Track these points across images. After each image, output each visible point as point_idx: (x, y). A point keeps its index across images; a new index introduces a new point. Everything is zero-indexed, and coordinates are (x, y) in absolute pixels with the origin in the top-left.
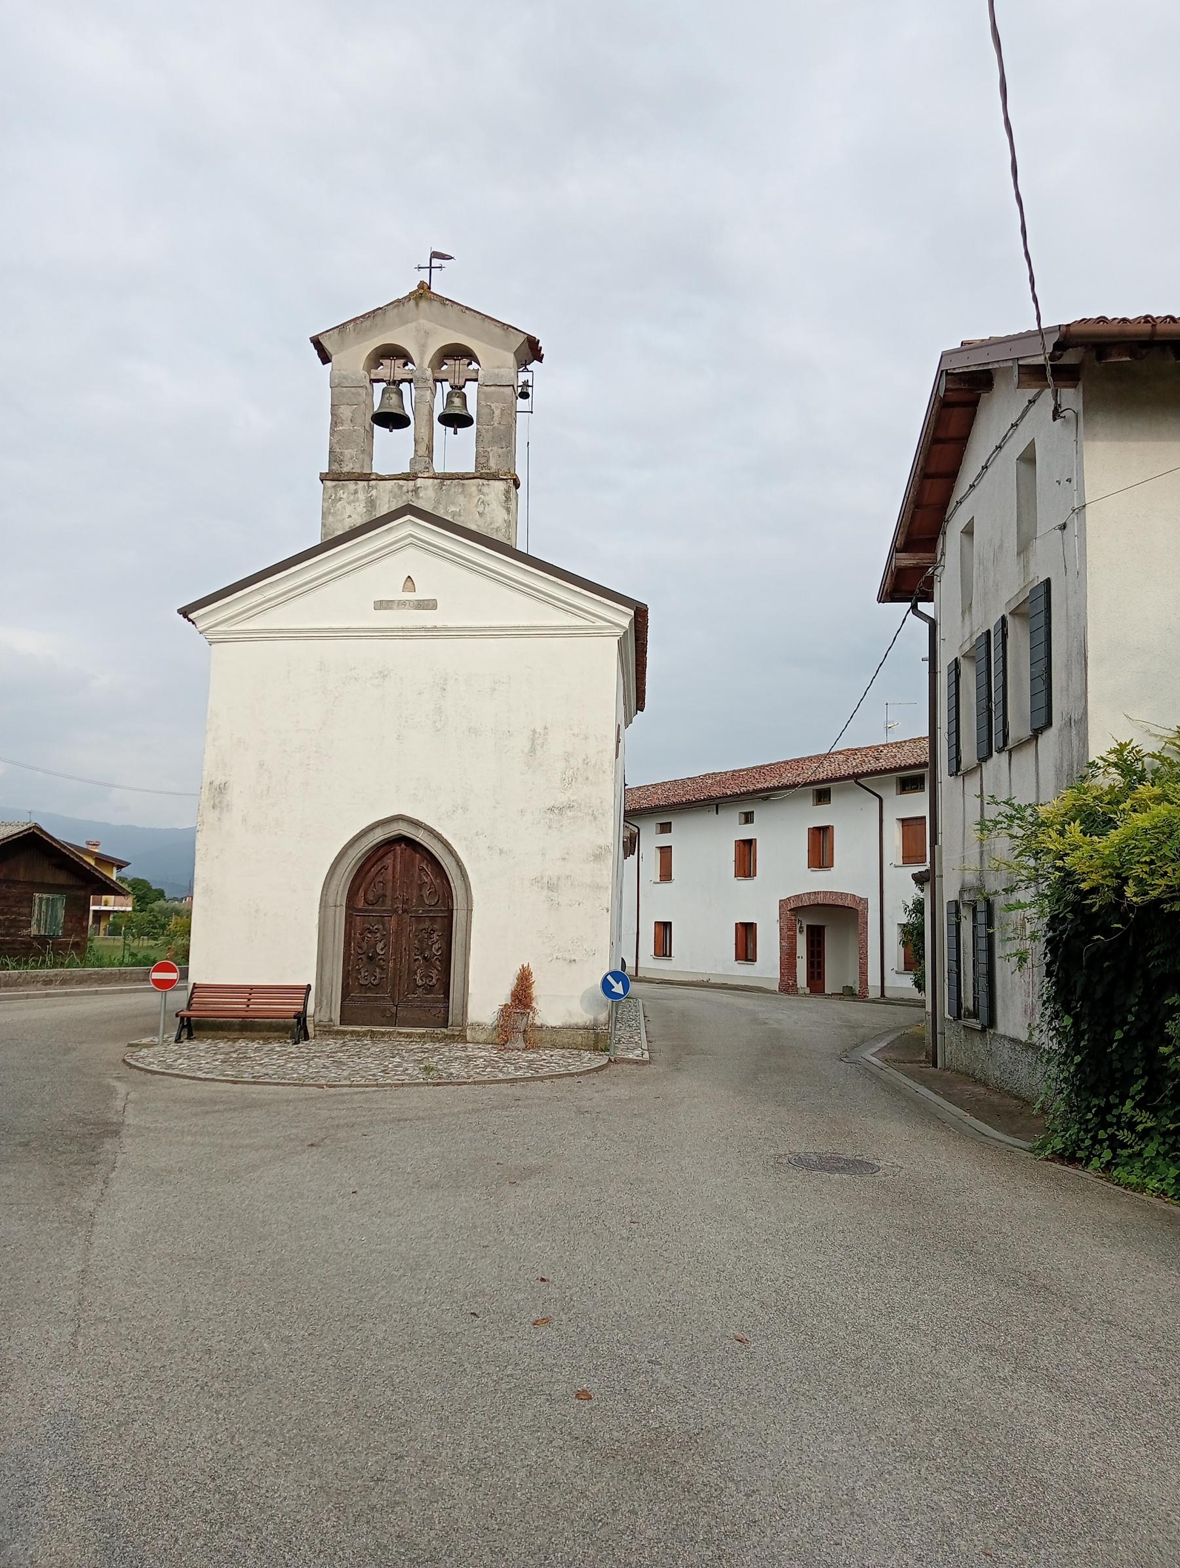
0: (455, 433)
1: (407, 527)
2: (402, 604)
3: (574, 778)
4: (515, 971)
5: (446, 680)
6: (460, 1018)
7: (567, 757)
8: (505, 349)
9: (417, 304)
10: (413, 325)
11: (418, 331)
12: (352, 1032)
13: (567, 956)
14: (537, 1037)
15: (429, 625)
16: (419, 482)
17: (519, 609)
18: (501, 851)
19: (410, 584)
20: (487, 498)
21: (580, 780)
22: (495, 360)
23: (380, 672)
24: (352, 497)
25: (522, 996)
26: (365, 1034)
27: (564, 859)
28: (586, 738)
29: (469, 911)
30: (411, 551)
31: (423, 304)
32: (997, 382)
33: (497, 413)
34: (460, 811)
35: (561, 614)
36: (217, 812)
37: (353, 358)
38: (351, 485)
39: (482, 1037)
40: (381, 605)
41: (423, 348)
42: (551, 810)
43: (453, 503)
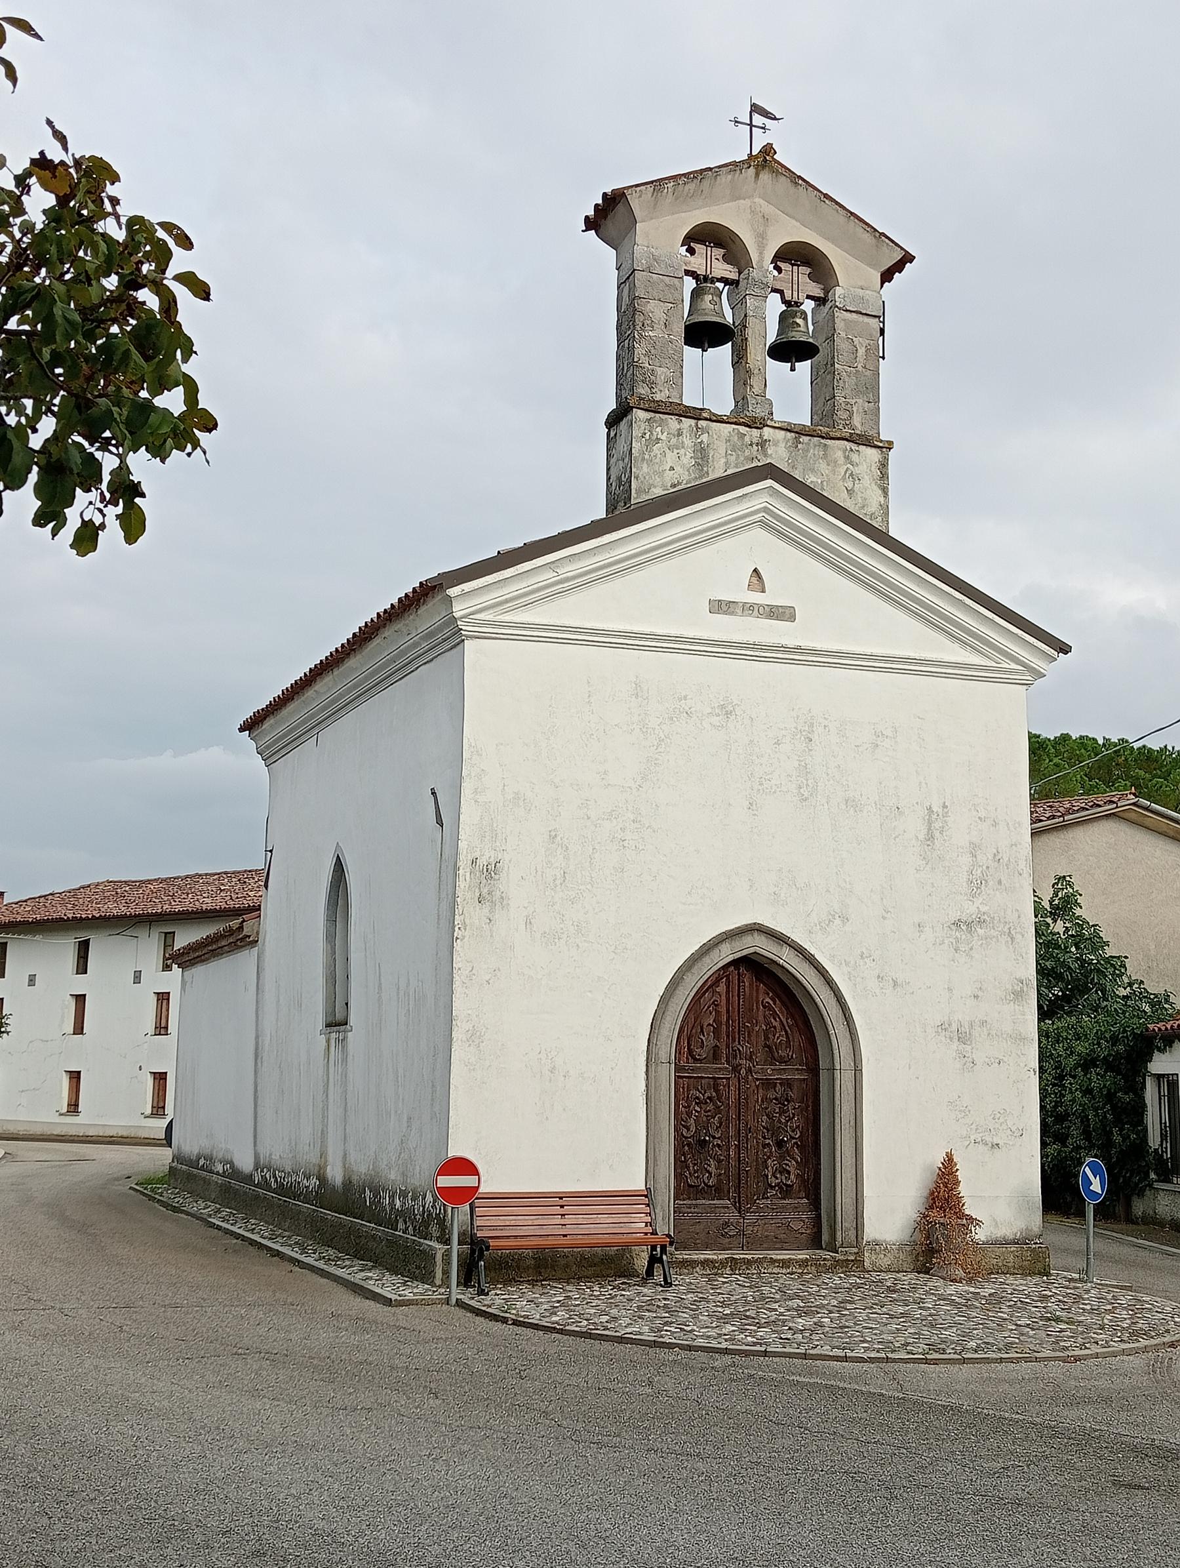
0: (793, 369)
2: (749, 609)
4: (939, 1159)
5: (812, 725)
6: (852, 1233)
7: (974, 849)
8: (869, 265)
9: (757, 175)
10: (748, 202)
12: (705, 1263)
13: (988, 1139)
14: (982, 1265)
15: (791, 643)
16: (767, 432)
17: (910, 637)
18: (895, 983)
19: (755, 580)
20: (856, 470)
21: (991, 883)
22: (852, 276)
23: (722, 707)
24: (674, 441)
25: (943, 1195)
26: (723, 1264)
27: (976, 997)
28: (995, 824)
29: (858, 1071)
30: (759, 533)
31: (765, 176)
33: (861, 351)
34: (838, 921)
36: (486, 910)
37: (660, 234)
38: (673, 422)
39: (885, 1262)
40: (720, 607)
41: (761, 238)
42: (957, 924)
43: (812, 470)
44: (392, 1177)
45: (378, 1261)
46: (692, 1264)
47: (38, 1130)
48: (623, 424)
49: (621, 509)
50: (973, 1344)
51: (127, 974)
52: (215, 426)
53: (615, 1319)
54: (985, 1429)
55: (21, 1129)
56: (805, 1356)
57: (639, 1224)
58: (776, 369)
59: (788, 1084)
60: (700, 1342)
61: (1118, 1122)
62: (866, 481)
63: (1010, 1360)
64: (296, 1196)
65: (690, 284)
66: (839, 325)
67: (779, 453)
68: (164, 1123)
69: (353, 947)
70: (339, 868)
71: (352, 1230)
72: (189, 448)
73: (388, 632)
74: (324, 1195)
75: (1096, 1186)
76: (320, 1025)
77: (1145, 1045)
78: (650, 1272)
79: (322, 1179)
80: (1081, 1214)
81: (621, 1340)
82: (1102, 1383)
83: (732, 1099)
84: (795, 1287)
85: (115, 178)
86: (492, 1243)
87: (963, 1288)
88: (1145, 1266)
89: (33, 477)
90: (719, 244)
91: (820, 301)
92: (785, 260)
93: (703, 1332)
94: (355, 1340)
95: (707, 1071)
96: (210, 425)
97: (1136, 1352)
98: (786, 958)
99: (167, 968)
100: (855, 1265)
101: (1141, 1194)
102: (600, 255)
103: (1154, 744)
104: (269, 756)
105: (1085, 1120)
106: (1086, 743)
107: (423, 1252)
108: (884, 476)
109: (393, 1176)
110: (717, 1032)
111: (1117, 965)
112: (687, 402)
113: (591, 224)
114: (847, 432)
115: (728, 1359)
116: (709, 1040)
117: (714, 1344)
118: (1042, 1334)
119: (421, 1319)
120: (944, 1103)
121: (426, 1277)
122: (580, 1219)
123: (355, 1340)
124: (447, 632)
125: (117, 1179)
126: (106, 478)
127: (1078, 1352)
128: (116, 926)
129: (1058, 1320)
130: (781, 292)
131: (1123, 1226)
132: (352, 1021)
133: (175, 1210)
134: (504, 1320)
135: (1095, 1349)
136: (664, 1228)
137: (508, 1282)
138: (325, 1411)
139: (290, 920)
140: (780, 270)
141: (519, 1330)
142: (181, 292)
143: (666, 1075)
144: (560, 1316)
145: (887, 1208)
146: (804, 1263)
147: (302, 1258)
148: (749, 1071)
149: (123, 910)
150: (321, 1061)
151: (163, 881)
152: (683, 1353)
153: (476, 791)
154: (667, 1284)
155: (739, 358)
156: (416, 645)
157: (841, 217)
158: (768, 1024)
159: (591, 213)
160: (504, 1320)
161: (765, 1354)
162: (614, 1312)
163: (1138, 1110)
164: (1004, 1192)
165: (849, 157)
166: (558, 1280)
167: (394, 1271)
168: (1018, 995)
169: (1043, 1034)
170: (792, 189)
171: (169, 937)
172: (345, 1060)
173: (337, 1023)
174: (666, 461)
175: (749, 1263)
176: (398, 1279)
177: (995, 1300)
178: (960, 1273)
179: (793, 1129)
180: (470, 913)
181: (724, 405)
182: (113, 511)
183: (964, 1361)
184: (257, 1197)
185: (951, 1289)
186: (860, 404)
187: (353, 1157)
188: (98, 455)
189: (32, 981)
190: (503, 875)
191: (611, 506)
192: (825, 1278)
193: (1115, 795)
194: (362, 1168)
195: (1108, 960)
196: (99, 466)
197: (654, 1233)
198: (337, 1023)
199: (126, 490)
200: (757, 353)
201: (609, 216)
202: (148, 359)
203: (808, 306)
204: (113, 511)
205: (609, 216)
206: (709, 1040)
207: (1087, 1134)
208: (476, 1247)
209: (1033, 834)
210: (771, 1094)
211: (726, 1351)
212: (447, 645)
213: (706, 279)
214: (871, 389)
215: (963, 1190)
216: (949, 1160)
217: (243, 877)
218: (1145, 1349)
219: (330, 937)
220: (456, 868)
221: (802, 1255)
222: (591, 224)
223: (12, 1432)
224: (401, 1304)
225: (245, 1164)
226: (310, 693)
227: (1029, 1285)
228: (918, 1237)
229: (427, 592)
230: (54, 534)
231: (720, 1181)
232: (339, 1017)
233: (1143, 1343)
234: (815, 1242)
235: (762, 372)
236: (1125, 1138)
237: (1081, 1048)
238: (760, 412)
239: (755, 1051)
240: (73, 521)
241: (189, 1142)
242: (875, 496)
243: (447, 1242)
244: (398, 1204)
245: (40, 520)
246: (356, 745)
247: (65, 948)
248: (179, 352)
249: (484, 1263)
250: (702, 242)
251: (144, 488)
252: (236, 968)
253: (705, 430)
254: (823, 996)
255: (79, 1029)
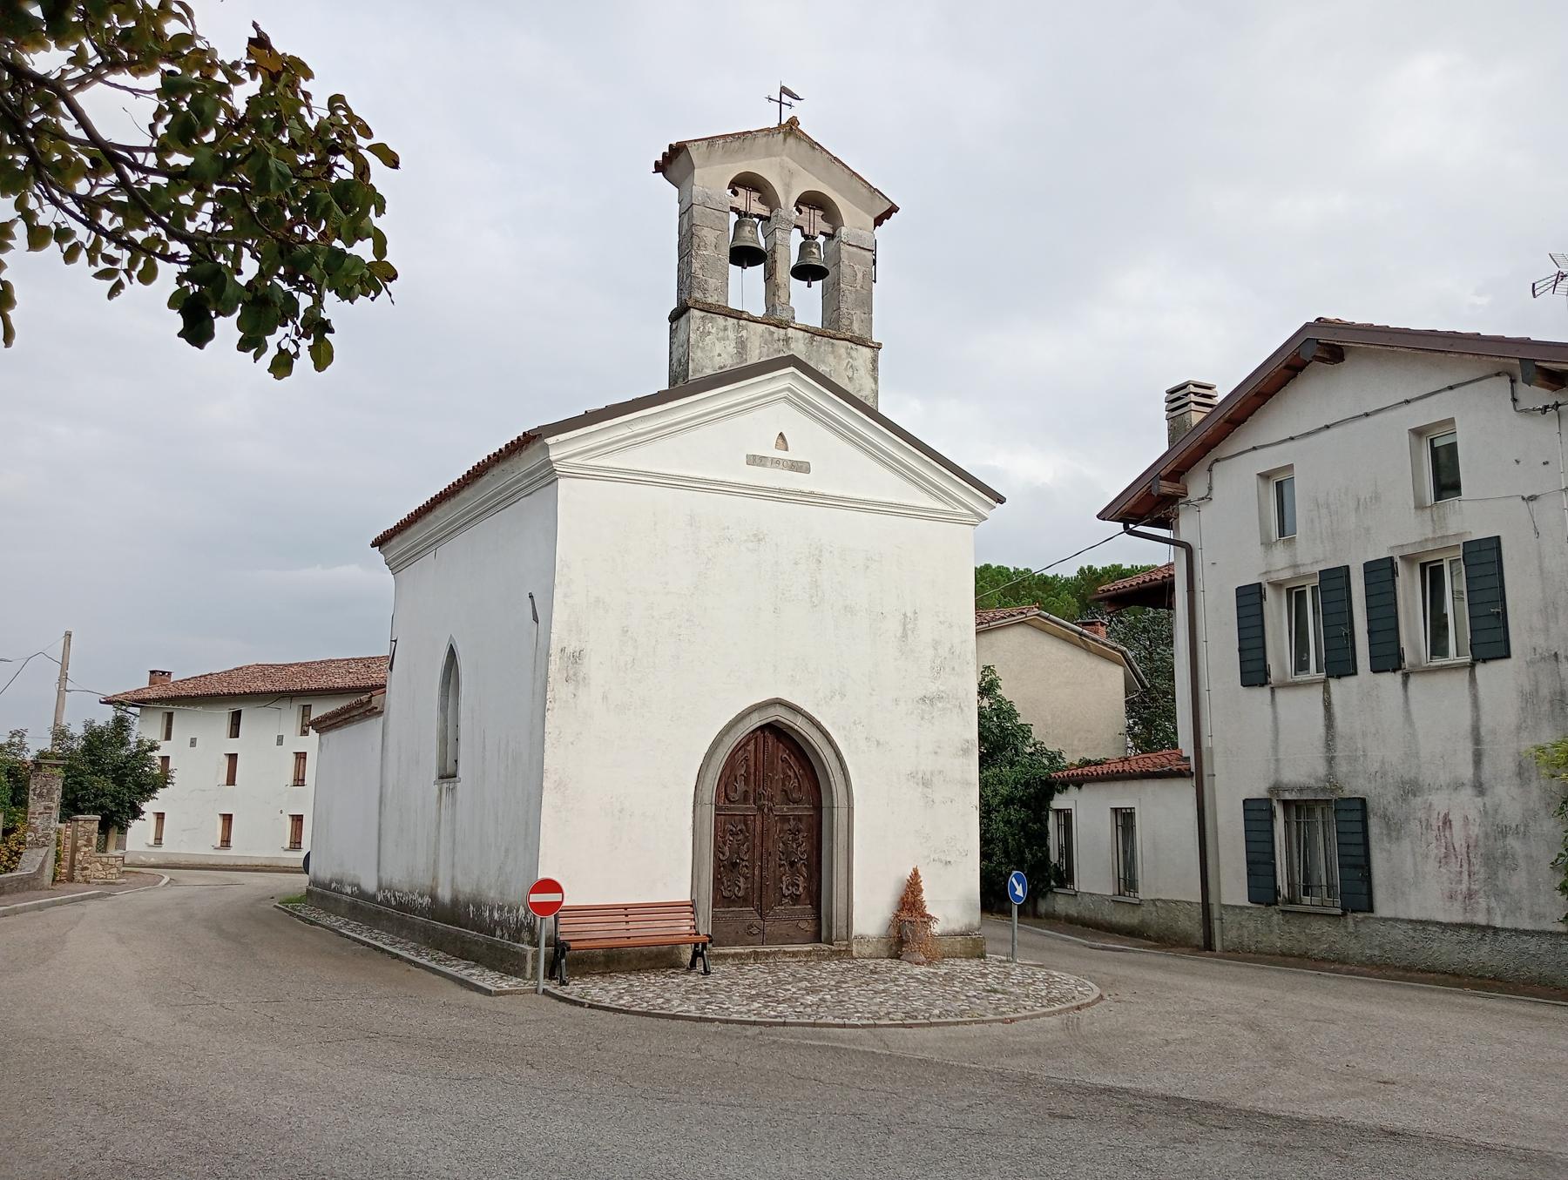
1: (785, 379)
3: (942, 668)
4: (909, 872)
7: (936, 644)
11: (782, 167)
12: (734, 956)
15: (807, 490)
17: (891, 488)
20: (855, 363)
22: (854, 220)
25: (910, 900)
26: (748, 956)
28: (951, 626)
29: (850, 809)
30: (783, 406)
31: (791, 141)
32: (1348, 359)
33: (860, 275)
35: (925, 495)
36: (572, 687)
37: (713, 179)
38: (720, 320)
39: (867, 951)
40: (754, 460)
41: (788, 187)
42: (923, 699)
44: (492, 894)
45: (478, 961)
46: (725, 956)
47: (197, 861)
48: (683, 320)
49: (680, 384)
50: (937, 1012)
51: (271, 740)
52: (396, 276)
53: (668, 1001)
54: (951, 1076)
55: (183, 861)
56: (814, 1025)
57: (685, 927)
58: (797, 285)
59: (798, 818)
60: (735, 1017)
61: (1029, 845)
62: (862, 371)
63: (965, 1023)
64: (412, 911)
65: (734, 217)
66: (844, 255)
67: (799, 348)
68: (302, 854)
69: (462, 715)
70: (452, 653)
71: (459, 938)
72: (372, 294)
73: (495, 471)
74: (437, 910)
75: (1019, 892)
76: (434, 777)
77: (1050, 788)
78: (693, 964)
79: (434, 897)
80: (1009, 913)
81: (674, 1017)
82: (1032, 1038)
83: (758, 829)
84: (803, 972)
85: (309, 75)
86: (572, 945)
87: (924, 969)
88: (1051, 950)
89: (238, 313)
90: (756, 190)
91: (830, 237)
92: (804, 204)
93: (737, 1010)
94: (465, 1024)
95: (739, 809)
96: (392, 275)
97: (1053, 1013)
98: (800, 724)
99: (305, 733)
100: (846, 954)
101: (1044, 896)
102: (666, 192)
103: (1049, 573)
104: (395, 567)
105: (1005, 841)
106: (1001, 571)
107: (517, 953)
108: (875, 369)
109: (492, 895)
110: (747, 782)
111: (1025, 731)
112: (732, 305)
113: (659, 167)
114: (848, 334)
115: (756, 1029)
116: (741, 786)
117: (745, 1018)
118: (985, 1002)
119: (516, 1004)
120: (910, 832)
121: (518, 972)
122: (641, 925)
123: (465, 1024)
124: (544, 472)
125: (263, 899)
126: (302, 314)
127: (1012, 1015)
128: (264, 700)
129: (995, 991)
130: (801, 228)
131: (1031, 920)
132: (461, 774)
133: (312, 923)
134: (582, 1005)
135: (1025, 1013)
136: (705, 929)
137: (584, 974)
138: (444, 1082)
139: (411, 698)
140: (800, 212)
141: (594, 1012)
142: (373, 161)
143: (709, 812)
144: (626, 1000)
145: (869, 911)
146: (808, 953)
147: (418, 959)
148: (770, 809)
149: (270, 687)
150: (434, 806)
151: (301, 665)
152: (723, 1026)
153: (565, 596)
154: (707, 972)
155: (769, 276)
156: (518, 481)
157: (846, 176)
158: (784, 773)
159: (660, 159)
160: (582, 1005)
161: (784, 1024)
162: (667, 995)
163: (1044, 834)
164: (953, 897)
165: (857, 129)
166: (623, 972)
167: (492, 968)
168: (966, 752)
169: (984, 784)
170: (810, 152)
171: (306, 710)
172: (454, 804)
173: (448, 776)
174: (715, 348)
175: (767, 955)
176: (496, 975)
177: (949, 978)
178: (922, 958)
179: (802, 851)
180: (558, 690)
181: (759, 310)
182: (305, 344)
183: (931, 1024)
184: (379, 912)
185: (917, 970)
186: (857, 315)
187: (460, 878)
188: (295, 294)
189: (193, 743)
190: (586, 661)
191: (673, 380)
192: (824, 964)
193: (1025, 608)
194: (467, 888)
195: (1019, 727)
196: (295, 304)
197: (697, 934)
198: (448, 776)
199: (317, 327)
200: (783, 273)
201: (673, 162)
202: (346, 212)
203: (821, 239)
204: (305, 344)
205: (673, 162)
206: (741, 786)
207: (1006, 853)
208: (559, 949)
209: (978, 633)
210: (786, 827)
211: (755, 1023)
212: (545, 482)
213: (746, 214)
214: (866, 303)
215: (925, 896)
216: (916, 873)
217: (367, 662)
218: (1060, 1012)
219: (443, 708)
220: (548, 655)
221: (808, 948)
222: (659, 167)
223: (183, 1107)
224: (498, 994)
225: (370, 885)
226: (430, 517)
227: (973, 965)
228: (894, 933)
229: (528, 440)
230: (256, 358)
231: (747, 893)
232: (449, 771)
233: (1058, 1007)
234: (817, 938)
235: (787, 286)
236: (1034, 856)
237: (1004, 790)
238: (785, 316)
239: (774, 792)
240: (272, 352)
241: (323, 869)
242: (868, 383)
243: (537, 945)
244: (496, 916)
245: (243, 346)
246: (466, 560)
247: (223, 716)
248: (373, 208)
249: (565, 960)
250: (744, 187)
251: (333, 324)
252: (360, 737)
253: (744, 328)
254: (826, 753)
255: (231, 780)
